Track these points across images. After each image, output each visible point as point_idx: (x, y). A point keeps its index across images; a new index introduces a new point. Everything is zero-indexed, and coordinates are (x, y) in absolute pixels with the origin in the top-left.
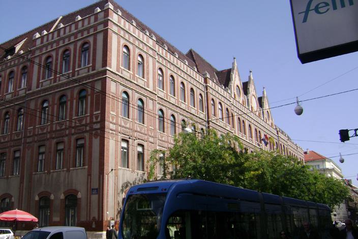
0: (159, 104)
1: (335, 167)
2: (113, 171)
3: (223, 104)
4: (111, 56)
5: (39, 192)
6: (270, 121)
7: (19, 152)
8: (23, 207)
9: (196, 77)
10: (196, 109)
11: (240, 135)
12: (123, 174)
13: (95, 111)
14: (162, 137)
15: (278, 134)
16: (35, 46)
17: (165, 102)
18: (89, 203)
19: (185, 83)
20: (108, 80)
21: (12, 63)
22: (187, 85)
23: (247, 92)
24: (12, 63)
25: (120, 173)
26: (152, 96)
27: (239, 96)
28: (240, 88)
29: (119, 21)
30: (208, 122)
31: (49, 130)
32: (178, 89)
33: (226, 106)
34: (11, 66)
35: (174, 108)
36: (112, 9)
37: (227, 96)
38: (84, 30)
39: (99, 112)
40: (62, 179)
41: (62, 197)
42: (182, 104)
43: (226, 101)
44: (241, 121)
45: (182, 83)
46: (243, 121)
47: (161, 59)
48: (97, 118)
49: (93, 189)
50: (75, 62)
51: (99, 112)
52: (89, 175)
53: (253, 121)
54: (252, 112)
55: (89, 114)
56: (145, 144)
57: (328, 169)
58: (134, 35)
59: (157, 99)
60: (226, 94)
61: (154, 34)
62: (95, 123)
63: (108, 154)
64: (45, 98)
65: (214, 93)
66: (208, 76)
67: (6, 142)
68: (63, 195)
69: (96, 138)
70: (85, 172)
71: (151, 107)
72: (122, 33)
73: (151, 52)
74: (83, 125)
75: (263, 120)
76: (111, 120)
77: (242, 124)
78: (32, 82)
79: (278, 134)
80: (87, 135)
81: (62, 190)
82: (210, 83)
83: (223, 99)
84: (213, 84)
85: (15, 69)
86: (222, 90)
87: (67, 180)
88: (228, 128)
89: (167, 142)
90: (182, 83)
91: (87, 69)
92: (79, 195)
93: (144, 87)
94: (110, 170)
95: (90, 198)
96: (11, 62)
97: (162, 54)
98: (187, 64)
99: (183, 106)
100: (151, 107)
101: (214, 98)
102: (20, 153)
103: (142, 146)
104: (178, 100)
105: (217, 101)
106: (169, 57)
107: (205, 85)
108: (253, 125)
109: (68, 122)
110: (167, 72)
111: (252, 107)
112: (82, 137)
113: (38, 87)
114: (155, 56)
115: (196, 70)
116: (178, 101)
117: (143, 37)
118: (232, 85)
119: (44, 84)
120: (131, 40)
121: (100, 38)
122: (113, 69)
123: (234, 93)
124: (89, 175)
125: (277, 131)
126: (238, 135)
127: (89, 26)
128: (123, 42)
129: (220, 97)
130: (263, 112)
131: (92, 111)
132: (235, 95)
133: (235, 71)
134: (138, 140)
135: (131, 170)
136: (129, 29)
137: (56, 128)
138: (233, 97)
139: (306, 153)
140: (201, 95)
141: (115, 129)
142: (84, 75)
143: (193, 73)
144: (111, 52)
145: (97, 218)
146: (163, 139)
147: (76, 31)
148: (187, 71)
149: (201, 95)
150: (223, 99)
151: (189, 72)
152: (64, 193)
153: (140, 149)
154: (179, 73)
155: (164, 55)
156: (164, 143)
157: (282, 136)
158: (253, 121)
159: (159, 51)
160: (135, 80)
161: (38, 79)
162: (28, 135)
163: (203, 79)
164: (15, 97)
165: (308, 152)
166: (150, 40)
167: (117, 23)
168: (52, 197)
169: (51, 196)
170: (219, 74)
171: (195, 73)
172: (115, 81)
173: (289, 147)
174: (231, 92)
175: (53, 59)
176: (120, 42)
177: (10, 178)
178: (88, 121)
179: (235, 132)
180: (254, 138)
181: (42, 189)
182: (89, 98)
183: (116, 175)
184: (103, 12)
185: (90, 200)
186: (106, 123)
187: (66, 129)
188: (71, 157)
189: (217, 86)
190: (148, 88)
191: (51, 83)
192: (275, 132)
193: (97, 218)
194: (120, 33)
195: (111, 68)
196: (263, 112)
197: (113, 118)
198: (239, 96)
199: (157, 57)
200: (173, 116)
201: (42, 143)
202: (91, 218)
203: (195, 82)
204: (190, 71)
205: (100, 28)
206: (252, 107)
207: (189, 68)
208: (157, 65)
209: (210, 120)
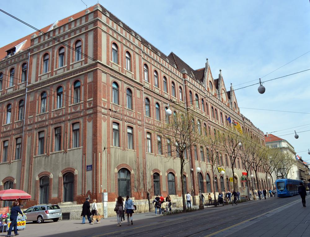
0: (145, 93)
1: (290, 146)
2: (106, 149)
3: (199, 95)
4: (101, 51)
5: (40, 173)
6: (237, 110)
7: (21, 138)
8: (24, 188)
9: (176, 73)
10: (177, 99)
11: (213, 120)
12: (115, 152)
13: (88, 99)
14: (149, 121)
15: (243, 120)
16: (33, 45)
17: (151, 92)
18: (84, 177)
19: (167, 77)
20: (99, 71)
21: (13, 61)
22: (169, 79)
23: (218, 87)
24: (13, 61)
25: (112, 151)
26: (140, 87)
27: (212, 89)
28: (212, 83)
29: (108, 22)
30: (187, 109)
31: (47, 118)
32: (161, 82)
33: (201, 97)
34: (11, 64)
35: (159, 97)
36: (101, 10)
37: (201, 87)
38: (77, 29)
39: (92, 99)
40: (60, 159)
41: (61, 175)
42: (165, 95)
43: (201, 93)
44: (214, 110)
45: (165, 77)
46: (216, 109)
47: (146, 57)
48: (90, 104)
49: (87, 166)
50: (70, 57)
51: (92, 99)
52: (84, 154)
53: (223, 110)
54: (222, 102)
55: (82, 102)
56: (134, 126)
57: (284, 148)
58: (122, 35)
59: (143, 89)
60: (201, 87)
61: (159, 52)
62: (89, 109)
63: (101, 135)
64: (44, 90)
65: (191, 86)
66: (186, 72)
67: (9, 131)
68: (61, 173)
69: (90, 122)
70: (81, 151)
71: (138, 95)
72: (111, 32)
73: (137, 50)
74: (78, 112)
75: (232, 109)
76: (103, 106)
77: (206, 106)
78: (31, 76)
79: (243, 120)
80: (81, 120)
81: (61, 169)
82: (188, 78)
83: (199, 91)
84: (190, 79)
85: (15, 66)
86: (198, 84)
87: (64, 160)
88: (204, 115)
89: (154, 125)
90: (165, 77)
91: (80, 63)
92: (76, 172)
93: (132, 78)
94: (103, 149)
95: (85, 174)
96: (11, 60)
97: (147, 52)
98: (168, 62)
99: (166, 96)
100: (138, 95)
101: (192, 90)
102: (22, 139)
103: (132, 128)
104: (161, 90)
105: (194, 93)
106: (152, 55)
107: (184, 79)
108: (223, 113)
109: (64, 110)
110: (151, 68)
111: (222, 99)
112: (78, 121)
113: (36, 80)
114: (141, 54)
115: (176, 67)
116: (162, 92)
117: (130, 37)
118: (206, 80)
119: (42, 78)
120: (119, 39)
121: (91, 37)
122: (104, 62)
123: (208, 87)
124: (84, 154)
125: (243, 118)
126: (212, 120)
127: (81, 25)
128: (111, 40)
129: (196, 90)
130: (231, 103)
131: (85, 99)
132: (208, 88)
133: (208, 70)
134: (128, 123)
135: (122, 148)
136: (117, 29)
137: (54, 115)
138: (221, 101)
139: (266, 136)
140: (180, 87)
141: (106, 113)
142: (77, 68)
143: (173, 69)
144: (101, 48)
145: (91, 191)
146: (150, 123)
147: (69, 30)
148: (169, 67)
149: (180, 87)
150: (199, 91)
151: (170, 68)
152: (61, 172)
153: (130, 131)
154: (162, 68)
155: (175, 72)
156: (151, 126)
157: (247, 122)
158: (223, 110)
159: (144, 50)
160: (123, 73)
161: (37, 74)
162: (29, 123)
163: (182, 74)
164: (16, 91)
165: (267, 136)
166: (136, 40)
167: (138, 53)
168: (51, 176)
169: (50, 176)
170: (196, 72)
171: (175, 69)
172: (106, 73)
173: (253, 131)
174: (206, 86)
175: (50, 56)
176: (109, 40)
177: (12, 162)
178: (82, 108)
179: (209, 118)
180: (225, 123)
181: (42, 170)
182: (83, 88)
183: (109, 153)
184: (93, 14)
185: (85, 176)
186: (99, 108)
187: (63, 115)
188: (68, 139)
189: (193, 81)
190: (136, 80)
191: (48, 77)
192: (242, 119)
193: (91, 191)
194: (109, 32)
195: (101, 60)
196: (231, 103)
197: (104, 104)
198: (212, 89)
199: (142, 55)
200: (157, 103)
201: (42, 129)
202: (86, 192)
203: (175, 77)
204: (170, 68)
205: (91, 27)
206: (222, 99)
207: (170, 66)
208: (143, 62)
209: (188, 107)
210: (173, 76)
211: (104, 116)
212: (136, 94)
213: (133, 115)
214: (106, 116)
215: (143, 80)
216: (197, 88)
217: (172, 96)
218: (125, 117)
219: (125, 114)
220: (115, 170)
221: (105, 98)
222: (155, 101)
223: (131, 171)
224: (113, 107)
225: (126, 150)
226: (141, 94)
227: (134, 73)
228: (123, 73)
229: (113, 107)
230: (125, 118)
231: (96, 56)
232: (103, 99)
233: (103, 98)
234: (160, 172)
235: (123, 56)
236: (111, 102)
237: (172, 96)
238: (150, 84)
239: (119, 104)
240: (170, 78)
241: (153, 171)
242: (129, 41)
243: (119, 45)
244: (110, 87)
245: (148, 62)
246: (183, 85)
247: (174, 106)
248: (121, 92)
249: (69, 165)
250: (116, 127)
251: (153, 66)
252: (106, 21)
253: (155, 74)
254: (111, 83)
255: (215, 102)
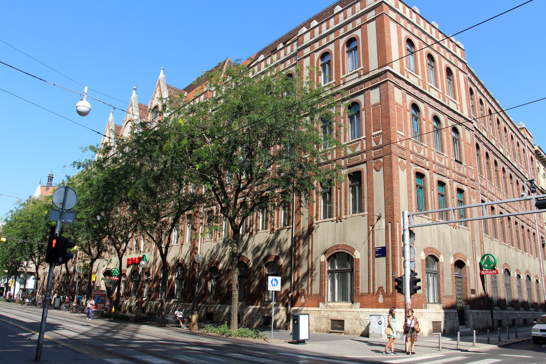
10: (440, 91)
72: (402, 22)
92: (357, 255)
121: (372, 28)
122: (396, 69)
160: (404, 75)
210: (448, 55)
211: (401, 162)
213: (445, 162)
214: (405, 161)
216: (444, 47)
217: (448, 96)
220: (421, 254)
221: (401, 131)
222: (431, 112)
223: (438, 257)
224: (415, 148)
225: (457, 228)
228: (404, 75)
229: (414, 146)
231: (383, 59)
234: (439, 254)
237: (448, 96)
239: (443, 152)
240: (443, 59)
241: (455, 256)
242: (417, 27)
247: (465, 121)
249: (344, 239)
252: (394, 5)
255: (449, 51)
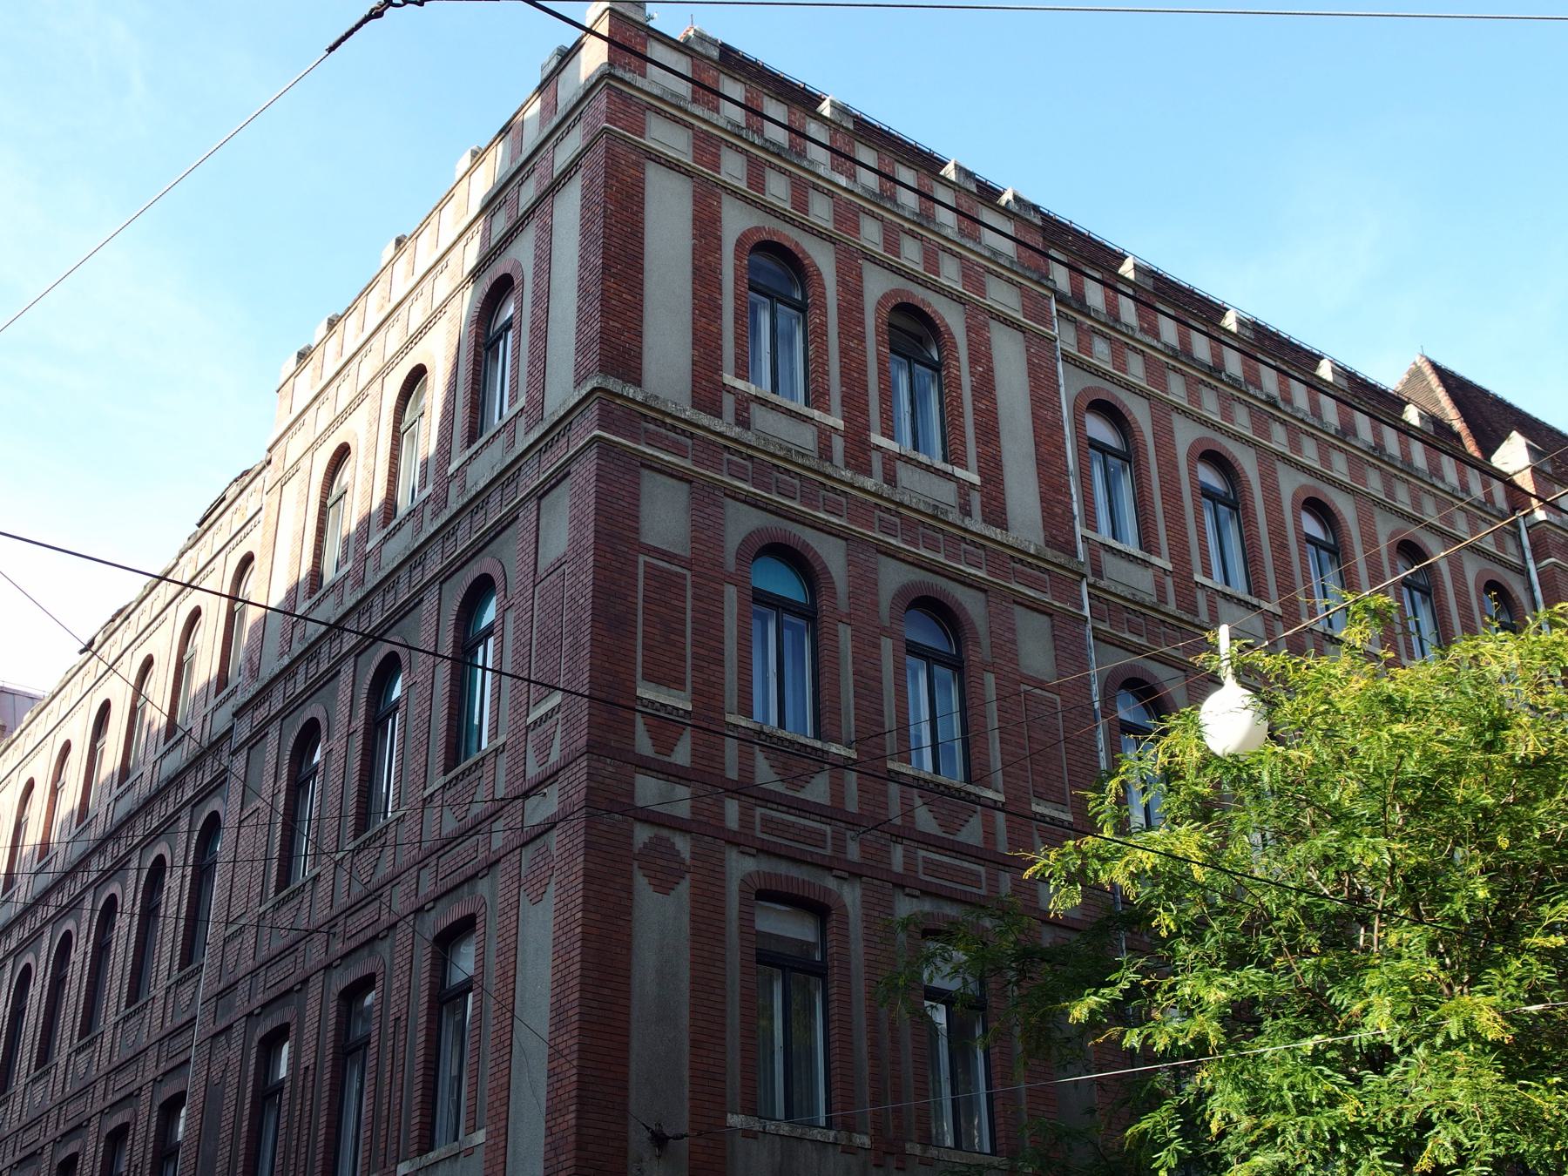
22: (1365, 521)
135: (864, 1140)
167: (1249, 433)
211: (655, 843)
212: (1006, 647)
215: (1079, 530)
218: (898, 855)
219: (732, 774)
226: (1068, 649)
227: (981, 474)
230: (898, 857)
232: (646, 692)
233: (648, 677)
235: (861, 338)
236: (730, 718)
238: (1163, 562)
243: (1344, 506)
244: (731, 592)
245: (1238, 437)
246: (1523, 572)
248: (845, 634)
250: (794, 928)
251: (1281, 468)
253: (1312, 527)
254: (739, 555)
